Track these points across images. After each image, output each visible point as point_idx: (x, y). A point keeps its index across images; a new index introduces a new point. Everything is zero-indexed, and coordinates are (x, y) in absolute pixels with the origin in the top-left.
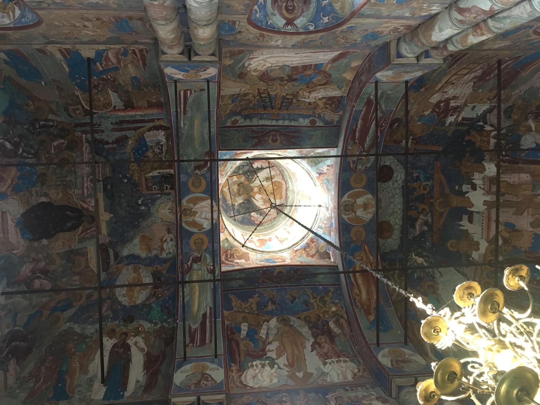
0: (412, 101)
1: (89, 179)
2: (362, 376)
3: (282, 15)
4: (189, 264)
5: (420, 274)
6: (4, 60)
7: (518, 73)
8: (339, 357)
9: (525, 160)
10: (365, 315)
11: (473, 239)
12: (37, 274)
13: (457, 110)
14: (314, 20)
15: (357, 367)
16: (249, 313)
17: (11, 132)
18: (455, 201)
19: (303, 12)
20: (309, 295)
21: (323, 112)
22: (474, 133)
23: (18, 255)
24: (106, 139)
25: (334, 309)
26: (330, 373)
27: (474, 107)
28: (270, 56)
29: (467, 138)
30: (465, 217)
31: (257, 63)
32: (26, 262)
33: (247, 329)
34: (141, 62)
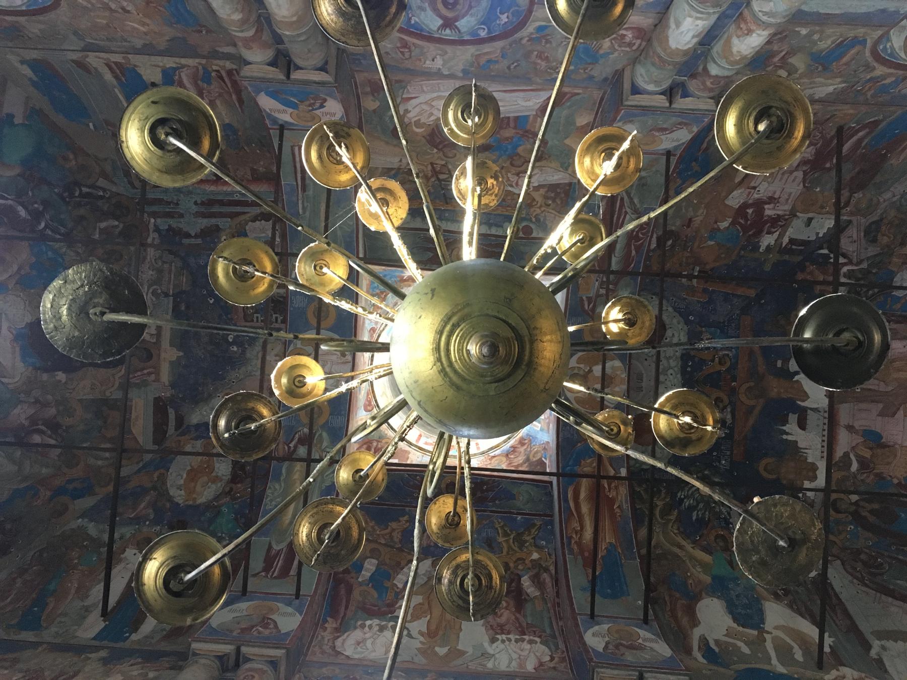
0: (695, 202)
1: (151, 291)
2: (554, 668)
3: (436, 10)
4: (292, 445)
5: (704, 514)
6: (30, 79)
7: (884, 158)
8: (523, 633)
9: (901, 316)
10: (584, 566)
11: (806, 459)
12: (37, 425)
13: (777, 222)
14: (487, 21)
15: (550, 654)
16: (385, 545)
17: (30, 193)
18: (776, 388)
19: (470, 7)
20: (497, 529)
21: (542, 212)
22: (811, 267)
23: (10, 386)
24: (186, 229)
25: (535, 556)
26: (497, 656)
27: (810, 220)
28: (435, 95)
29: (800, 276)
30: (793, 418)
31: (417, 110)
32: (21, 401)
33: (374, 569)
34: (234, 97)
